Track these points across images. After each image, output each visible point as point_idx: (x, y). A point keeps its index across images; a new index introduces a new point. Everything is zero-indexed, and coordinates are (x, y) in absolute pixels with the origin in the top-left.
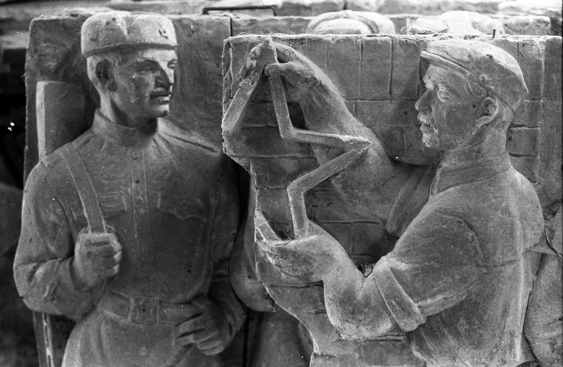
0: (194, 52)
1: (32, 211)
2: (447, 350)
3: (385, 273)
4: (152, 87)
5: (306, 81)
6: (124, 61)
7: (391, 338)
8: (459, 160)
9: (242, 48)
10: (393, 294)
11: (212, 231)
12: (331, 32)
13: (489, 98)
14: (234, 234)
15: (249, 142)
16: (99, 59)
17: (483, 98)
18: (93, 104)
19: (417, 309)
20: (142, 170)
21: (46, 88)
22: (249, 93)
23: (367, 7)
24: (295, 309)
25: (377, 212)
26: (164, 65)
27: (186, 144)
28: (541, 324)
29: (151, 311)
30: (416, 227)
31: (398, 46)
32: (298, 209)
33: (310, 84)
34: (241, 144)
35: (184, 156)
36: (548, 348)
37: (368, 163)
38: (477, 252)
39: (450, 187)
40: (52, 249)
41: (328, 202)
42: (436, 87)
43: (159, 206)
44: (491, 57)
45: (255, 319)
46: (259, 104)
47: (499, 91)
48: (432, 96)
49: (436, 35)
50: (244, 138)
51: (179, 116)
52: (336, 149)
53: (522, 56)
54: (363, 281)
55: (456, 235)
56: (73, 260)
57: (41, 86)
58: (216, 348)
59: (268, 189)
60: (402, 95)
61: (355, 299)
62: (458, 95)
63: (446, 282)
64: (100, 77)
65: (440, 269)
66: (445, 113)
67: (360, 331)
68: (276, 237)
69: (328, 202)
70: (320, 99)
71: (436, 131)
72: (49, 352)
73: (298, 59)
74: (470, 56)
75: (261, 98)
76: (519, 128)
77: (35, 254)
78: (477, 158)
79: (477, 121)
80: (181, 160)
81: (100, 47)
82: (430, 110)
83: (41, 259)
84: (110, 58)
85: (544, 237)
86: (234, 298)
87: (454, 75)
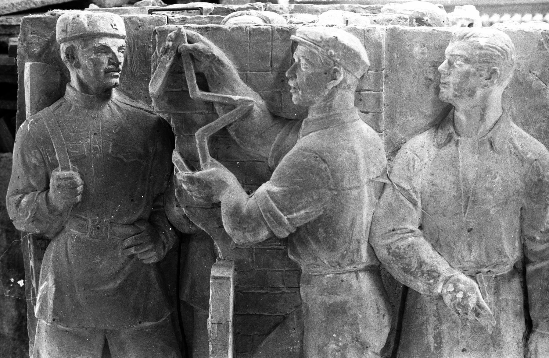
0: (140, 42)
1: (19, 155)
2: (311, 252)
3: (263, 193)
4: (105, 65)
5: (208, 56)
6: (86, 46)
7: (276, 247)
8: (317, 113)
9: (163, 33)
10: (270, 210)
11: (151, 173)
12: (235, 24)
13: (336, 67)
14: (168, 175)
15: (169, 102)
16: (68, 45)
17: (331, 68)
18: (66, 79)
19: (286, 220)
20: (98, 126)
21: (31, 67)
22: (168, 65)
23: (281, 11)
24: (204, 225)
25: (260, 152)
26: (115, 50)
27: (133, 108)
28: (380, 234)
29: (104, 228)
30: (286, 161)
31: (276, 32)
32: (203, 149)
33: (210, 59)
34: (164, 103)
35: (128, 116)
36: (385, 252)
37: (253, 116)
38: (329, 179)
39: (311, 132)
40: (33, 183)
41: (228, 146)
42: (299, 60)
43: (110, 151)
44: (336, 38)
45: (184, 239)
46: (176, 74)
47: (343, 62)
48: (297, 66)
49: (304, 25)
50: (166, 99)
51: (129, 88)
52: (230, 105)
53: (367, 39)
54: (248, 199)
55: (313, 167)
56: (48, 191)
57: (28, 65)
58: (152, 258)
59: (184, 136)
60: (279, 68)
61: (241, 212)
62: (313, 65)
63: (307, 201)
64: (68, 58)
65: (302, 191)
66: (305, 79)
67: (246, 237)
68: (187, 169)
69: (228, 146)
70: (218, 70)
71: (300, 92)
72: (31, 263)
73: (201, 41)
74: (321, 37)
75: (178, 70)
76: (367, 92)
77: (21, 188)
78: (329, 112)
79: (328, 84)
80: (127, 119)
81: (68, 36)
82: (296, 77)
83: (26, 191)
84: (76, 44)
85: (385, 171)
86: (166, 222)
87: (311, 51)
